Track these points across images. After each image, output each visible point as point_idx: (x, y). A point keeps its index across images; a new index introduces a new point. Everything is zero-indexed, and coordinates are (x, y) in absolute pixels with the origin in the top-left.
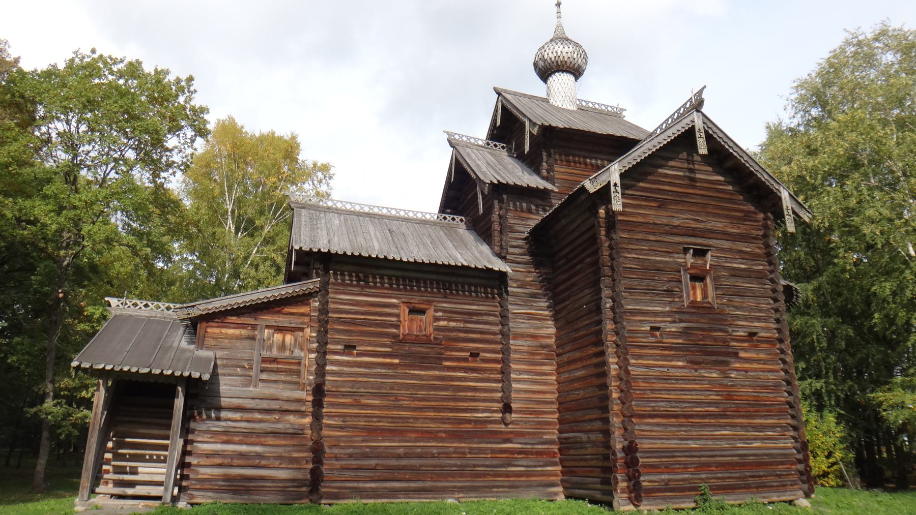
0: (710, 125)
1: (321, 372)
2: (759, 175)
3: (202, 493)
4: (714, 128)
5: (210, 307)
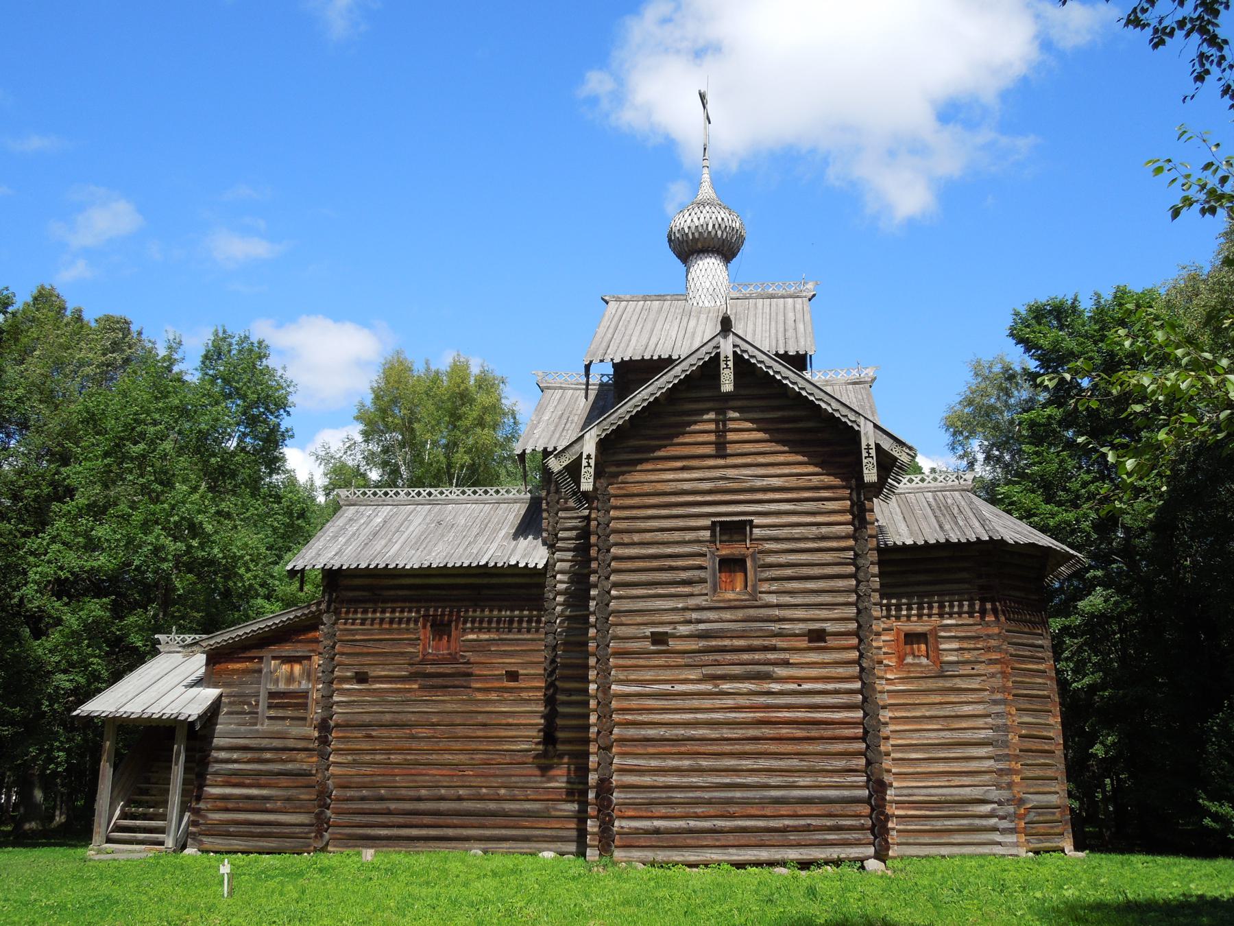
0: (745, 346)
1: (327, 702)
2: (824, 406)
3: (210, 840)
4: (750, 349)
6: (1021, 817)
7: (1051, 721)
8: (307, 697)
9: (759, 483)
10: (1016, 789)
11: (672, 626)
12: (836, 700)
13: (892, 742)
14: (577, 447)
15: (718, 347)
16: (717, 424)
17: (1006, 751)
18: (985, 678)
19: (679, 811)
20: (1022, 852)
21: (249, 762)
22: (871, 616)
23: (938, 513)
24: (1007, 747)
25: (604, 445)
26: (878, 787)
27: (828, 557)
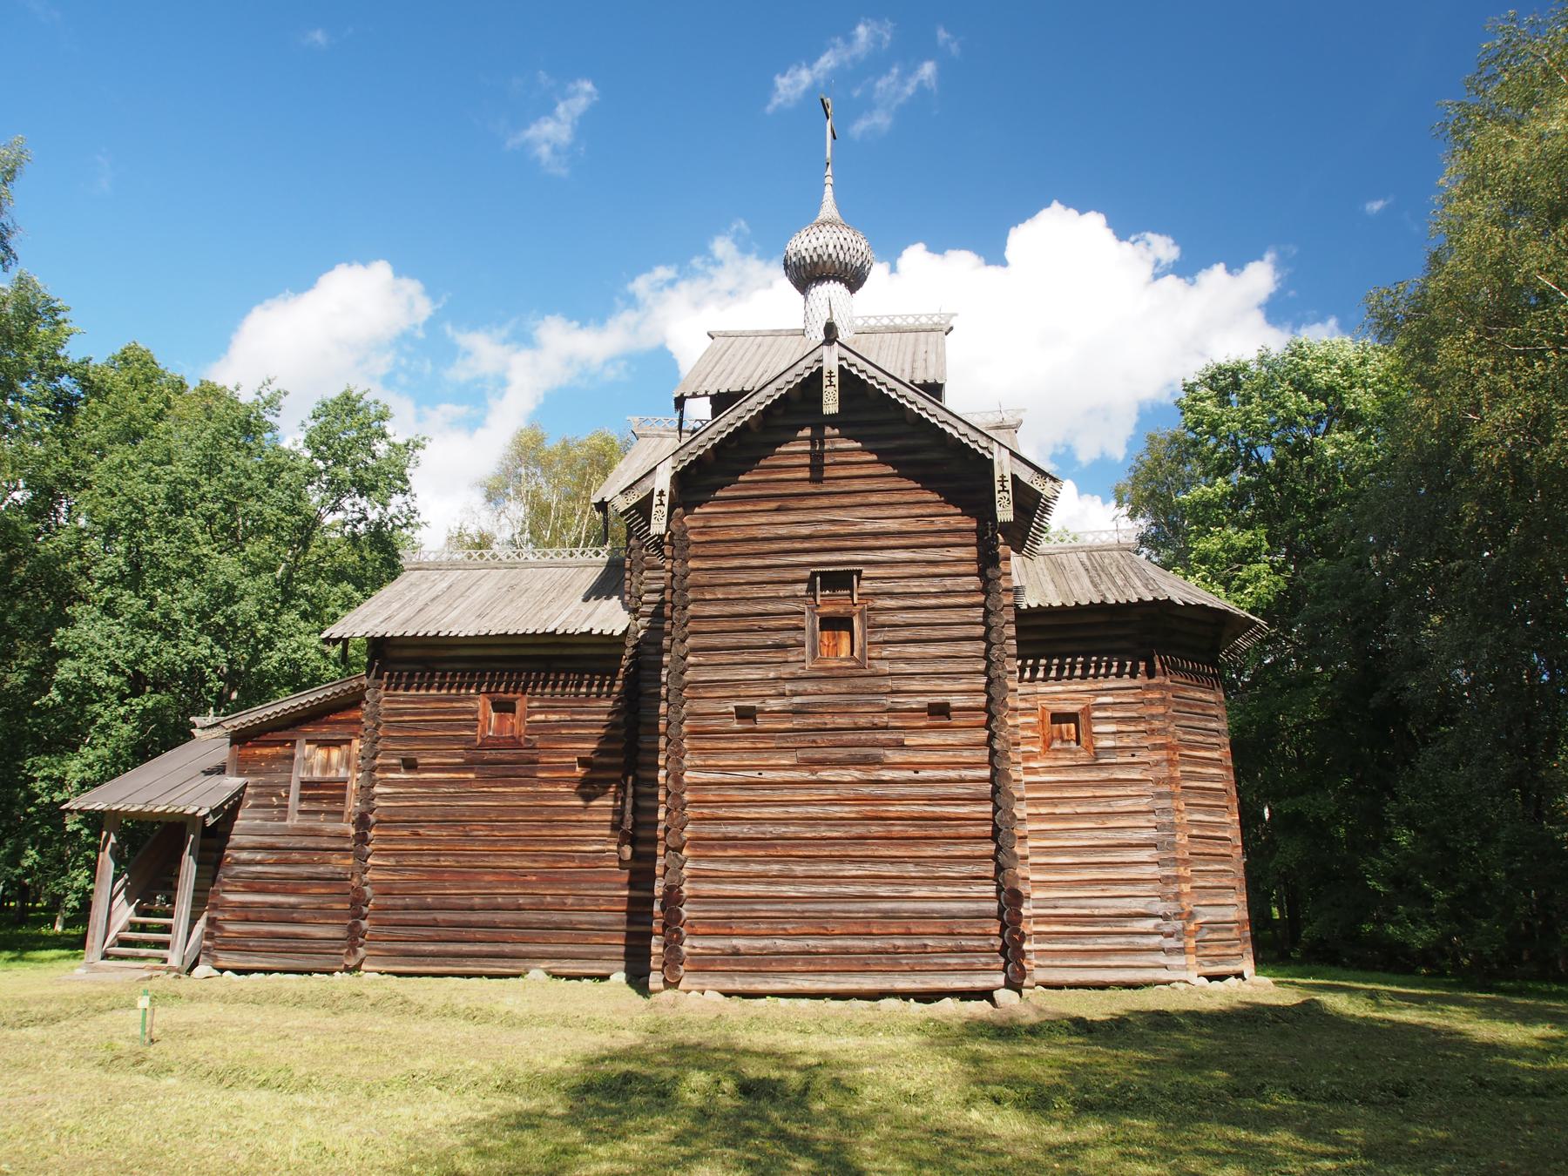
0: (853, 359)
2: (949, 429)
5: (236, 723)
6: (1191, 934)
7: (1228, 819)
8: (344, 787)
9: (869, 527)
10: (1185, 901)
11: (761, 700)
12: (961, 791)
13: (1031, 843)
14: (647, 483)
15: (821, 361)
16: (813, 444)
17: (1172, 855)
18: (1147, 766)
19: (763, 927)
20: (1192, 976)
21: (276, 863)
22: (1006, 687)
23: (1093, 573)
24: (1175, 849)
25: (679, 479)
26: (1011, 899)
27: (953, 616)
